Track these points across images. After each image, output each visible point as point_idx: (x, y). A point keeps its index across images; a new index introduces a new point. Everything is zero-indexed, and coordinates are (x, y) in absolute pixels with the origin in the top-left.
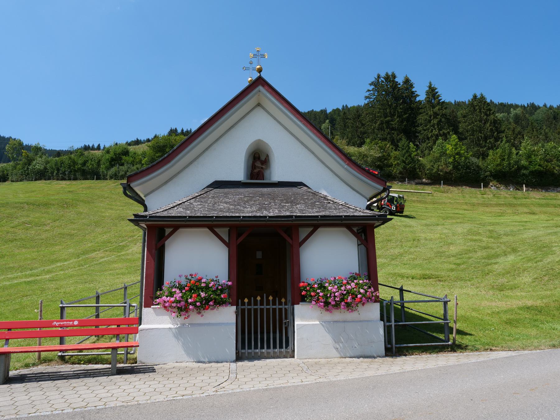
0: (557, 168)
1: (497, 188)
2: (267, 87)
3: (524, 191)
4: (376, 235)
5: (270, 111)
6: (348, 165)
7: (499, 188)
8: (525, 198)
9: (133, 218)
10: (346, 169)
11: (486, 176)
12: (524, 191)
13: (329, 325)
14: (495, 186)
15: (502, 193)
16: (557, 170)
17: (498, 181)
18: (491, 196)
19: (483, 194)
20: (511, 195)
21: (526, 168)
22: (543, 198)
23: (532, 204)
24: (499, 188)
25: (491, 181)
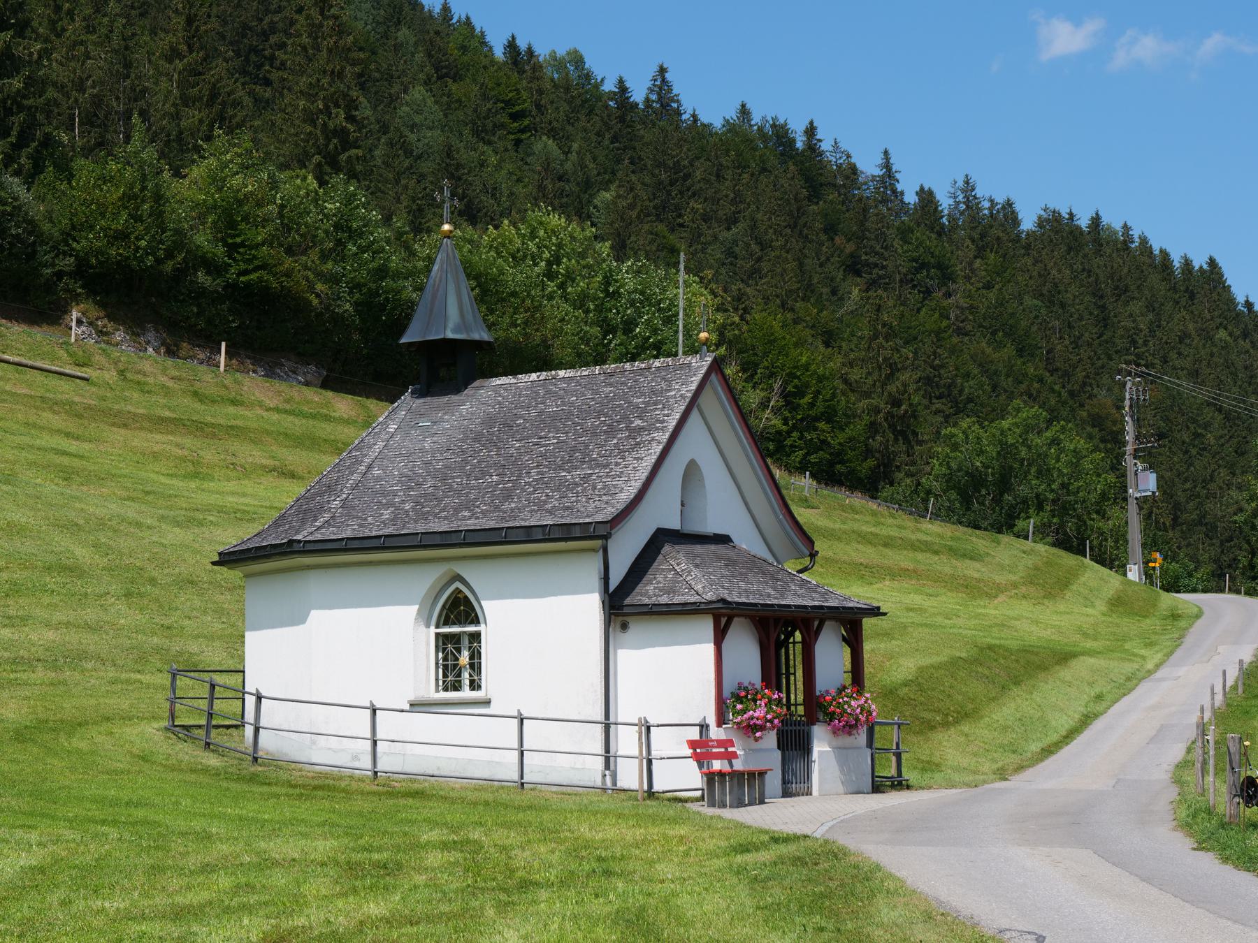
0: (319, 287)
1: (101, 333)
2: (720, 376)
3: (222, 368)
4: (864, 627)
5: (706, 414)
6: (783, 515)
7: (106, 334)
8: (234, 402)
9: (216, 558)
10: (780, 522)
11: (60, 275)
12: (222, 368)
13: (838, 749)
14: (91, 324)
15: (146, 366)
16: (318, 296)
17: (102, 305)
18: (111, 376)
19: (81, 361)
20: (179, 379)
21: (214, 268)
22: (288, 407)
23: (916, 572)
24: (106, 334)
25: (76, 298)
